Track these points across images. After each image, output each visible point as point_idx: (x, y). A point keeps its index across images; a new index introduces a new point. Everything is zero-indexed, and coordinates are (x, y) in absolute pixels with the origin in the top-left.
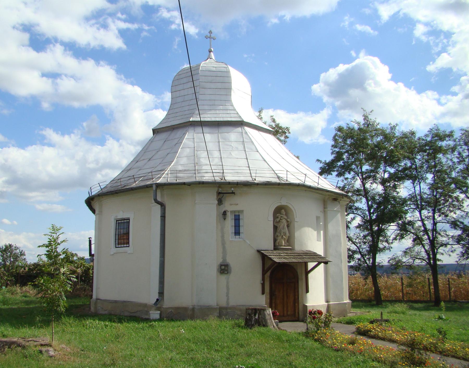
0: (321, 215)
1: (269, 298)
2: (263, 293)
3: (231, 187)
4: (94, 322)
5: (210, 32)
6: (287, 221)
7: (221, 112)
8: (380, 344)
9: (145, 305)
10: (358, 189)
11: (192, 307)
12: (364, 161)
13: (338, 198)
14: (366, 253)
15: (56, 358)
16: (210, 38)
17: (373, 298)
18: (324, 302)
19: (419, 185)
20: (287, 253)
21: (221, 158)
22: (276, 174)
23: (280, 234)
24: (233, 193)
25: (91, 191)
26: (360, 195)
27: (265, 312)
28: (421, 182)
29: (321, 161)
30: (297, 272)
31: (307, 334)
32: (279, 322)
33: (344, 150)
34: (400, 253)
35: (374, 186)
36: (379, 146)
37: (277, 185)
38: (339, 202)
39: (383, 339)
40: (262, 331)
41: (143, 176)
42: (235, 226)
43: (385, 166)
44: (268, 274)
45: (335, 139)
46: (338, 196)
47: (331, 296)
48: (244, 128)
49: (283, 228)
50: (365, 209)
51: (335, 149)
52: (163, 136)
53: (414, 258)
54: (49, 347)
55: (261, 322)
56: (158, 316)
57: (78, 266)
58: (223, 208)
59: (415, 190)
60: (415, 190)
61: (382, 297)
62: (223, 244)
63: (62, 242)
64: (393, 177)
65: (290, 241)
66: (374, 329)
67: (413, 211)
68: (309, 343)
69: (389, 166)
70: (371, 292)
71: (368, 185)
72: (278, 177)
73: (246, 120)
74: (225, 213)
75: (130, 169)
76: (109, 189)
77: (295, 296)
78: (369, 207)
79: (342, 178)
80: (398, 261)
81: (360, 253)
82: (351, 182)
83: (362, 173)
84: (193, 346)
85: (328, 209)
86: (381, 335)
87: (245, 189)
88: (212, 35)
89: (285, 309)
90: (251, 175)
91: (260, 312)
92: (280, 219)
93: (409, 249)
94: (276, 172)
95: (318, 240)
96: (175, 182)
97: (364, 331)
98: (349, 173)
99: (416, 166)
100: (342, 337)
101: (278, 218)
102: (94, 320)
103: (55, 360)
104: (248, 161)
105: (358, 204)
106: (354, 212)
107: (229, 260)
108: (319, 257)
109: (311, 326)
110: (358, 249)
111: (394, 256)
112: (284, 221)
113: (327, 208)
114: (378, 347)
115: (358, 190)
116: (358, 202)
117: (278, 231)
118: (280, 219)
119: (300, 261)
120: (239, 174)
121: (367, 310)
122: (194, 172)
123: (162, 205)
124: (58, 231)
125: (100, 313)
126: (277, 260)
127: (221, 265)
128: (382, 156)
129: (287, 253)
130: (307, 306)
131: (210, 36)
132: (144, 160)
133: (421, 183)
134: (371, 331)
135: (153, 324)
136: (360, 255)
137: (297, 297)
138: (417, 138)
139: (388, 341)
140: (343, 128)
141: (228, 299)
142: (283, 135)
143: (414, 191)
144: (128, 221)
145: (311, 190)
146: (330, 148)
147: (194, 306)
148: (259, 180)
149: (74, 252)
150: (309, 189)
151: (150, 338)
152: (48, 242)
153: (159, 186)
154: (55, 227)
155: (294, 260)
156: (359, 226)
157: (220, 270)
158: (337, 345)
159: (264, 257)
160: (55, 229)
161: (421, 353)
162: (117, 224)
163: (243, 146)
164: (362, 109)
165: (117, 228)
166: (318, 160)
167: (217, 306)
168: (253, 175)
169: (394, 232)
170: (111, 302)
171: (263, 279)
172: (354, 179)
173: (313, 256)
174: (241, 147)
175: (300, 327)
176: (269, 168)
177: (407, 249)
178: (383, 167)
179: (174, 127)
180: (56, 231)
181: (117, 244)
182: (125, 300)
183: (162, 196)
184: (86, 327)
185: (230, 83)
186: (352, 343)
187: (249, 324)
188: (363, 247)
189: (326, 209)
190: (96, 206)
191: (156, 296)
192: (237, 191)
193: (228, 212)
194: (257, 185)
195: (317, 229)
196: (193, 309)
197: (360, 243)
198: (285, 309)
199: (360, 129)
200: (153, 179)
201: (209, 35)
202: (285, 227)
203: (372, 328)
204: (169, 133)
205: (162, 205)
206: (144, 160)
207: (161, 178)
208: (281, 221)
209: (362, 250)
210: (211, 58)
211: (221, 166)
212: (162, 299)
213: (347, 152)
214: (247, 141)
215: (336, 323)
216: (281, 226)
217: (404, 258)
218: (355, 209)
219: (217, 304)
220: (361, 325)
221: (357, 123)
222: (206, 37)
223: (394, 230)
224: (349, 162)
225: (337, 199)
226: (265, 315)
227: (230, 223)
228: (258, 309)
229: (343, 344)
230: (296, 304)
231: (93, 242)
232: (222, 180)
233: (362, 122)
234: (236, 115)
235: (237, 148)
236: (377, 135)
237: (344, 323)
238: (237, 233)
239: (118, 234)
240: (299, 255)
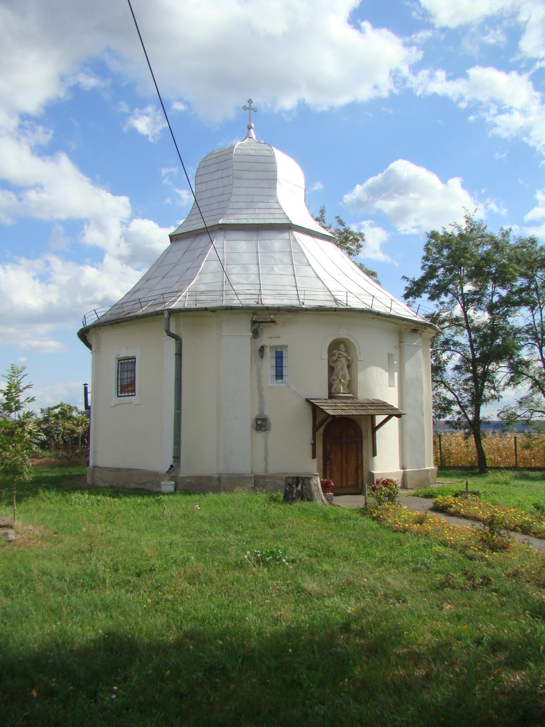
0: (396, 353)
1: (322, 463)
2: (314, 457)
3: (271, 314)
4: (83, 496)
5: (250, 101)
6: (348, 360)
7: (262, 211)
8: (455, 522)
9: (156, 474)
10: (457, 317)
11: (217, 475)
12: (466, 279)
13: (418, 329)
14: (467, 403)
15: (16, 543)
16: (250, 109)
17: (476, 464)
18: (399, 468)
19: (539, 313)
20: (346, 403)
21: (259, 274)
22: (333, 296)
23: (338, 377)
24: (273, 322)
25: (85, 320)
26: (461, 325)
27: (311, 481)
28: (542, 308)
29: (408, 278)
30: (361, 429)
31: (364, 511)
32: (334, 496)
33: (439, 264)
34: (514, 404)
35: (479, 313)
36: (487, 259)
37: (333, 311)
38: (420, 334)
39: (465, 517)
40: (306, 507)
41: (153, 299)
42: (276, 367)
43: (494, 286)
44: (321, 430)
45: (427, 250)
46: (419, 326)
47: (408, 462)
48: (292, 234)
49: (342, 369)
50: (466, 345)
51: (426, 263)
52: (183, 244)
53: (532, 411)
54: (10, 529)
55: (305, 495)
56: (172, 489)
57: (78, 423)
58: (260, 342)
59: (533, 318)
60: (533, 318)
61: (487, 462)
62: (260, 390)
63: (25, 388)
64: (506, 302)
65: (350, 386)
66: (455, 503)
67: (532, 347)
68: (366, 522)
69: (499, 286)
70: (473, 457)
71: (470, 312)
72: (336, 300)
73: (295, 222)
74: (262, 350)
75: (137, 291)
76: (109, 318)
77: (357, 460)
78: (472, 341)
79: (436, 302)
80: (511, 414)
81: (459, 403)
82: (449, 307)
83: (463, 295)
84: (206, 526)
85: (405, 343)
86: (463, 512)
87: (290, 316)
88: (253, 105)
89: (344, 478)
90: (298, 297)
91: (303, 482)
92: (338, 357)
93: (526, 398)
94: (333, 293)
95: (391, 385)
96: (194, 307)
97: (443, 506)
98: (446, 295)
99: (537, 286)
100: (408, 514)
101: (334, 355)
102: (83, 494)
103: (15, 545)
104: (295, 278)
105: (458, 337)
106: (450, 348)
107: (268, 412)
108: (390, 408)
109: (371, 500)
110: (456, 399)
111: (507, 408)
112: (343, 360)
113: (404, 342)
114: (451, 527)
115: (457, 319)
116: (458, 334)
117: (335, 372)
118: (338, 357)
119: (363, 413)
120: (282, 295)
121: (459, 480)
122: (220, 293)
123: (178, 339)
124: (20, 374)
125: (98, 485)
126: (331, 412)
127: (257, 420)
128: (490, 273)
129: (346, 403)
130: (373, 474)
131: (250, 106)
132: (156, 277)
133: (543, 309)
134: (451, 507)
135: (161, 498)
136: (458, 406)
137: (360, 461)
138: (538, 247)
139: (472, 519)
140: (437, 233)
141: (266, 465)
142: (355, 244)
143: (532, 320)
144: (134, 360)
145: (381, 317)
146: (421, 260)
147: (221, 474)
148: (309, 304)
149: (73, 405)
150: (378, 317)
151: (154, 517)
152: (8, 387)
153: (172, 312)
154: (15, 369)
155: (355, 413)
156: (457, 368)
157: (255, 426)
158: (399, 525)
159: (315, 409)
160: (15, 372)
161: (501, 535)
162: (120, 365)
163: (290, 258)
164: (463, 208)
165: (120, 370)
166: (404, 277)
167: (251, 473)
168: (301, 297)
169: (506, 375)
170: (112, 471)
171: (314, 438)
172: (453, 303)
173: (382, 407)
174: (287, 260)
175: (357, 501)
176: (323, 288)
177: (522, 398)
178: (491, 287)
179: (197, 232)
180: (17, 373)
181: (120, 393)
182: (131, 467)
183: (177, 326)
184: (70, 503)
185: (275, 171)
186: (421, 521)
187: (288, 498)
188: (463, 396)
189: (402, 344)
190: (92, 340)
191: (170, 461)
192: (279, 318)
193: (267, 347)
194: (335, 311)
195: (390, 370)
196: (219, 479)
197: (459, 390)
198: (344, 478)
199: (461, 236)
200: (164, 303)
201: (248, 106)
202: (344, 367)
203: (453, 502)
204: (192, 240)
205: (178, 339)
206: (156, 277)
207: (177, 302)
208: (339, 359)
209: (463, 400)
210: (250, 136)
211: (259, 285)
212: (178, 465)
213: (443, 266)
214: (296, 251)
215: (411, 497)
216: (339, 367)
217: (518, 410)
218: (453, 345)
219: (251, 471)
220: (439, 499)
221: (457, 227)
222: (245, 108)
223: (506, 373)
224: (446, 280)
225: (418, 330)
226: (310, 485)
227: (269, 361)
228: (301, 477)
229: (406, 523)
230: (360, 472)
231: (89, 389)
232: (258, 304)
233: (464, 226)
234: (282, 216)
235: (282, 261)
236: (483, 244)
237: (422, 497)
238: (279, 375)
239: (121, 379)
240: (362, 406)
